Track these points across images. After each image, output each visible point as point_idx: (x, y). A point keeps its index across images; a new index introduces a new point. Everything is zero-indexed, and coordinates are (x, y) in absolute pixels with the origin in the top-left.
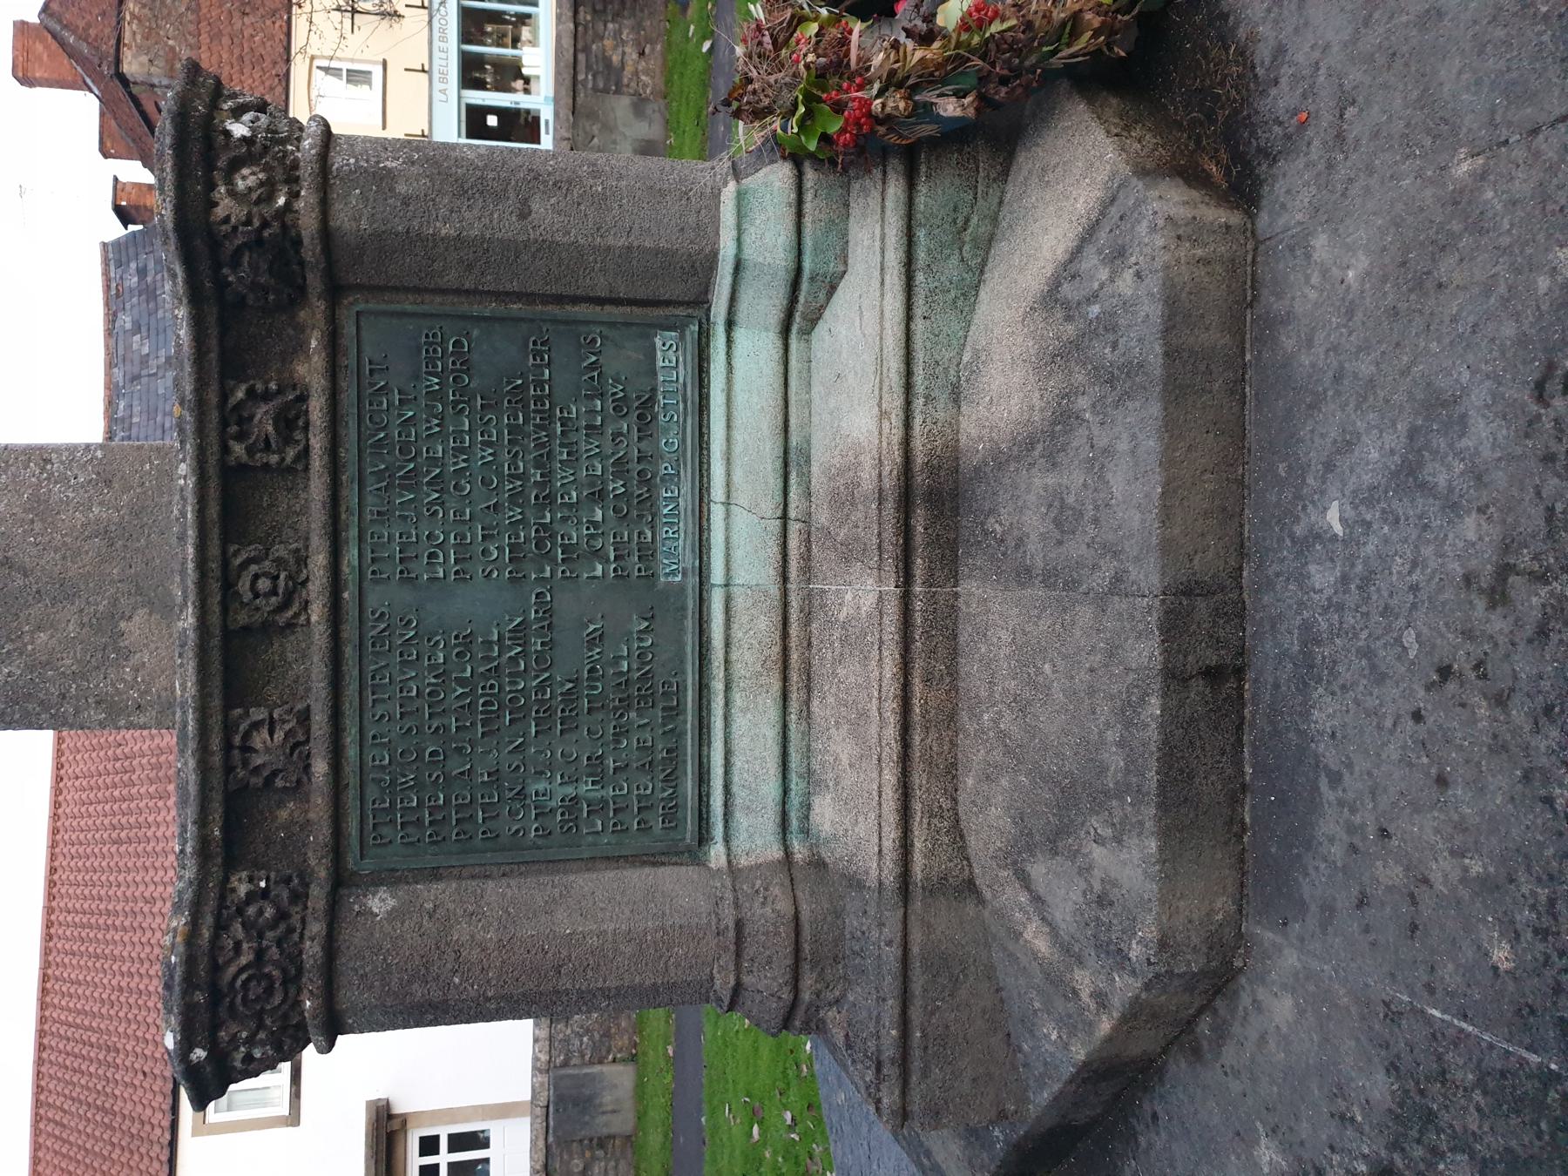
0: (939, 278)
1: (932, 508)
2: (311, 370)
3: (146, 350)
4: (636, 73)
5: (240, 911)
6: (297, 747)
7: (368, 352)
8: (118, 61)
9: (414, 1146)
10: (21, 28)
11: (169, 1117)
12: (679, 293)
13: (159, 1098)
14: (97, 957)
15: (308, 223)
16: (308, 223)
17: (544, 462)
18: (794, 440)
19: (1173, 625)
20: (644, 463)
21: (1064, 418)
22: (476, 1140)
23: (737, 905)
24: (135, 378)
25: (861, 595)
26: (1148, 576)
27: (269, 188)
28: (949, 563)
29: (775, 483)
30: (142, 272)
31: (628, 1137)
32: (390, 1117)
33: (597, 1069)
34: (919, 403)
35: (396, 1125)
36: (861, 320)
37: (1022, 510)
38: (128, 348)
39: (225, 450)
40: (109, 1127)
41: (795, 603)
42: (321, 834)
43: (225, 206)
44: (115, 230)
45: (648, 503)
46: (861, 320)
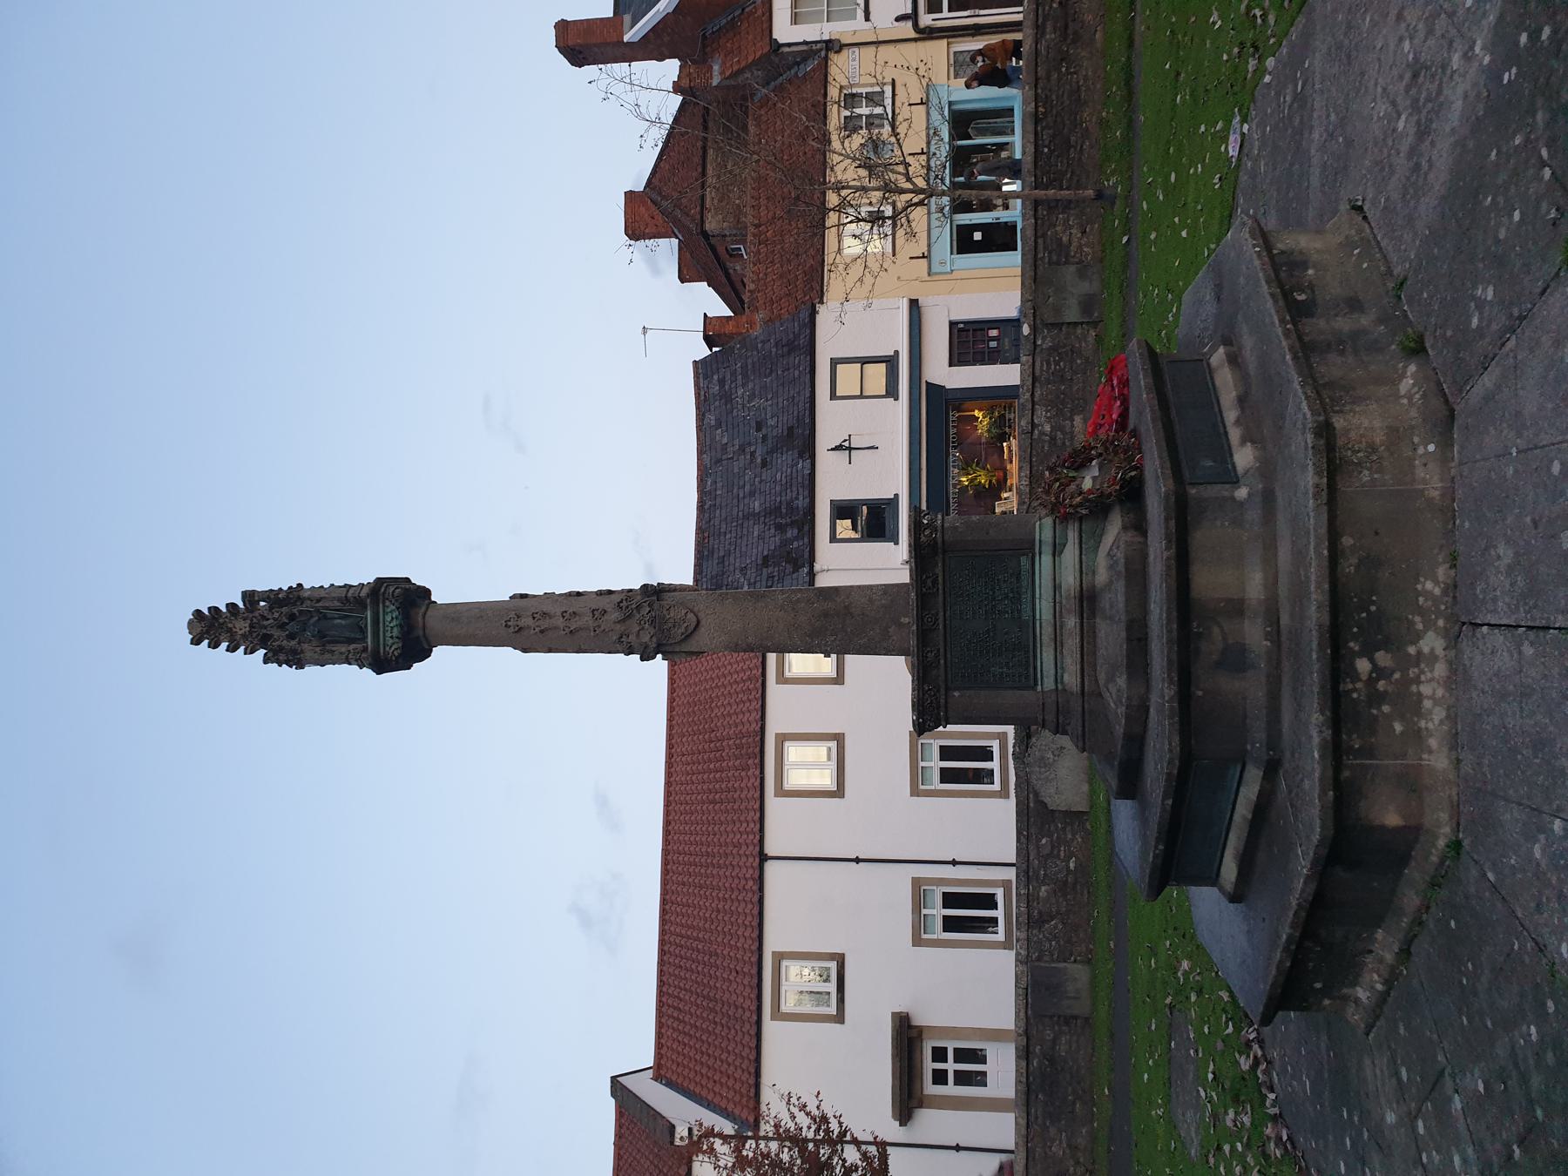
0: (1087, 547)
1: (1088, 600)
2: (939, 570)
3: (725, 440)
4: (1080, 246)
6: (937, 656)
8: (703, 222)
9: (928, 1054)
10: (630, 196)
11: (755, 1003)
12: (1028, 548)
13: (748, 990)
14: (701, 887)
15: (939, 540)
16: (939, 540)
17: (993, 590)
19: (1129, 628)
20: (1019, 587)
21: (1111, 582)
22: (977, 1056)
24: (719, 461)
25: (1071, 622)
26: (1123, 618)
28: (1093, 615)
30: (722, 382)
31: (1087, 1019)
32: (910, 1027)
33: (1062, 965)
35: (914, 1033)
36: (1070, 554)
37: (1105, 602)
38: (713, 439)
40: (712, 1010)
42: (942, 677)
43: (923, 538)
44: (703, 351)
45: (1019, 599)
46: (1070, 554)
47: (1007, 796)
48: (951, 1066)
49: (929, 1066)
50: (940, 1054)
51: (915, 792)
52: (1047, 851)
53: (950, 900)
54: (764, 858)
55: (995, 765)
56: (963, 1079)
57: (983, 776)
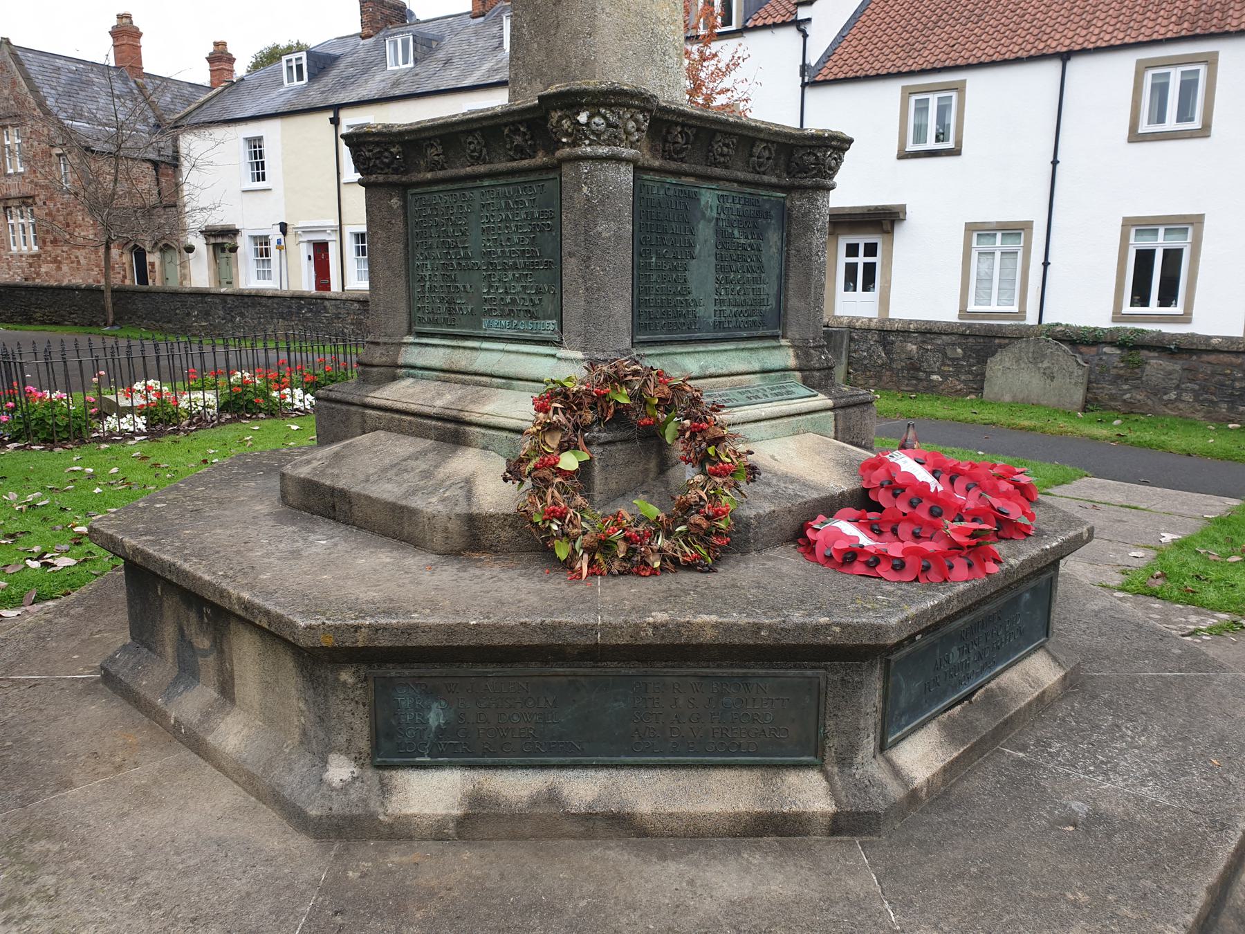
5: (386, 150)
7: (546, 184)
9: (871, 239)
15: (560, 153)
18: (514, 382)
22: (869, 284)
23: (385, 344)
27: (567, 134)
29: (501, 372)
32: (893, 223)
33: (844, 360)
34: (483, 431)
35: (887, 226)
39: (506, 125)
41: (466, 377)
43: (555, 115)
47: (1114, 320)
48: (861, 260)
49: (861, 240)
50: (871, 250)
51: (1128, 223)
52: (949, 353)
53: (1172, 257)
54: (1065, 57)
55: (1154, 307)
56: (851, 270)
57: (1141, 296)
